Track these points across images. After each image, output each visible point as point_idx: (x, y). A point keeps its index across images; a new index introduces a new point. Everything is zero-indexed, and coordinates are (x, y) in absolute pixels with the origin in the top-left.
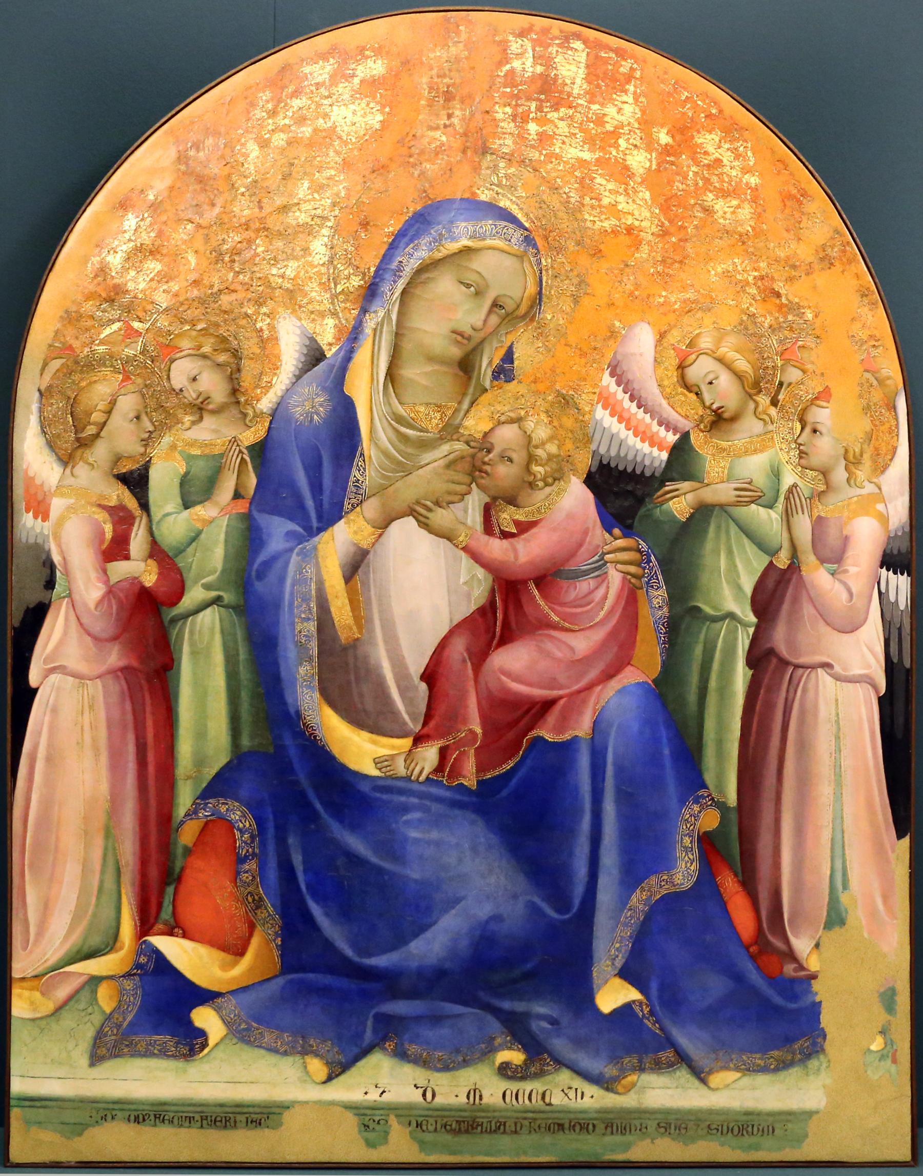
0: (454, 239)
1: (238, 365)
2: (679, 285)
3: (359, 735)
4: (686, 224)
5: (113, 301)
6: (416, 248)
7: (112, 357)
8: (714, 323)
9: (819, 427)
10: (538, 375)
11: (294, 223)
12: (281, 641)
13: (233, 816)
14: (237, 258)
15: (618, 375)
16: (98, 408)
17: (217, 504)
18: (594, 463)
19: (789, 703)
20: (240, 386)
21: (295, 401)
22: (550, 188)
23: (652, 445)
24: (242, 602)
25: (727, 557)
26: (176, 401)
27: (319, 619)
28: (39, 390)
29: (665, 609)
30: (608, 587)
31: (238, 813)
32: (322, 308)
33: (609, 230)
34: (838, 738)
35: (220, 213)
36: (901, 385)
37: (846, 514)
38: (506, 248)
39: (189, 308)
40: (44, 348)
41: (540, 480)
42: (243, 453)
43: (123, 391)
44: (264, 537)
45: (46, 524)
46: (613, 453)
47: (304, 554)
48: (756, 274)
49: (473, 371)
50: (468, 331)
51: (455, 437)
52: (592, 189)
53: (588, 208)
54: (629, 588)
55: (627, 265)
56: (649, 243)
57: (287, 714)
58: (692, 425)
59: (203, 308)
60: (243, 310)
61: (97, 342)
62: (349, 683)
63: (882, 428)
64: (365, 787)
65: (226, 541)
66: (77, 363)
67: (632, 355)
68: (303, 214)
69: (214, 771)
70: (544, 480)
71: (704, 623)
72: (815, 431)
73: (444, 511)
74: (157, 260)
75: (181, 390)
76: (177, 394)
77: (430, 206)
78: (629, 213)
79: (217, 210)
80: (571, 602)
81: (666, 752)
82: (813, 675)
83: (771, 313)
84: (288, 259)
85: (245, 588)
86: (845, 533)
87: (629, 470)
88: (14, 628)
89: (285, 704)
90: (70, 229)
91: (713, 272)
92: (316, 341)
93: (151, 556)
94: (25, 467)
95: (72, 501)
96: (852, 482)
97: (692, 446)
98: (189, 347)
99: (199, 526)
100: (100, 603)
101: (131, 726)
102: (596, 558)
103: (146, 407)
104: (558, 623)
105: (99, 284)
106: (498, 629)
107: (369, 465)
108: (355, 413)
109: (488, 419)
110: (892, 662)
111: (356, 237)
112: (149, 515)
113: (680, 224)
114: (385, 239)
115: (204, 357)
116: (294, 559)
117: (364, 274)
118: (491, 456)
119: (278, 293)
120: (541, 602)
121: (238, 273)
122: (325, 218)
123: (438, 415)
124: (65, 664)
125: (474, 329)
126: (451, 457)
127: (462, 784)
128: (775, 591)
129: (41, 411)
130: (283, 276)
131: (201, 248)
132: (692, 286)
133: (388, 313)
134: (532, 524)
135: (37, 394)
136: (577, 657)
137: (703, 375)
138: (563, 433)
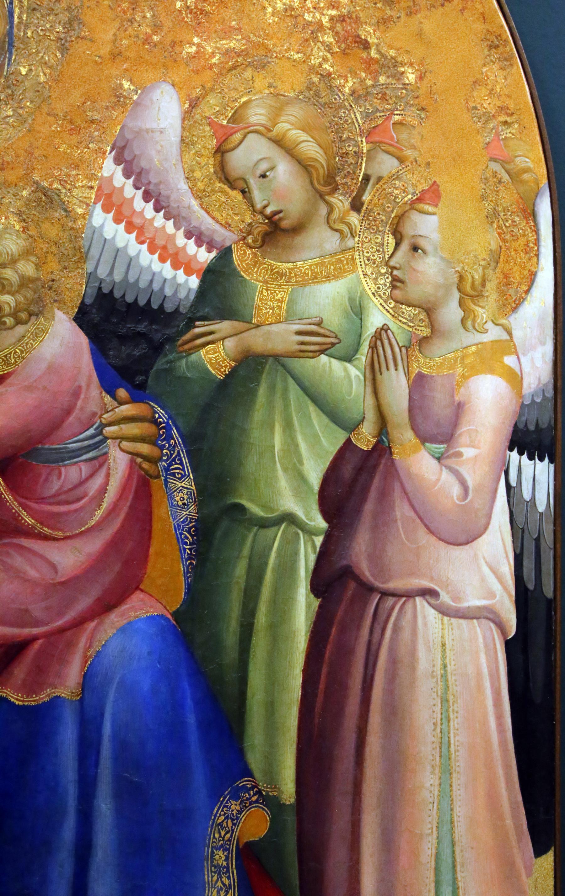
8: (270, 86)
9: (422, 243)
15: (126, 162)
18: (89, 291)
19: (374, 648)
23: (176, 266)
25: (284, 431)
29: (192, 508)
30: (108, 475)
34: (445, 700)
36: (545, 181)
37: (459, 370)
41: (9, 315)
48: (334, 12)
54: (140, 476)
58: (235, 238)
63: (515, 245)
70: (14, 314)
71: (249, 530)
72: (415, 248)
80: (54, 496)
81: (191, 719)
82: (409, 606)
83: (355, 74)
86: (457, 398)
87: (142, 302)
91: (270, 10)
96: (469, 323)
97: (235, 269)
102: (91, 431)
104: (33, 527)
110: (526, 589)
128: (355, 480)
132: (240, 29)
136: (60, 579)
137: (251, 164)
138: (45, 247)
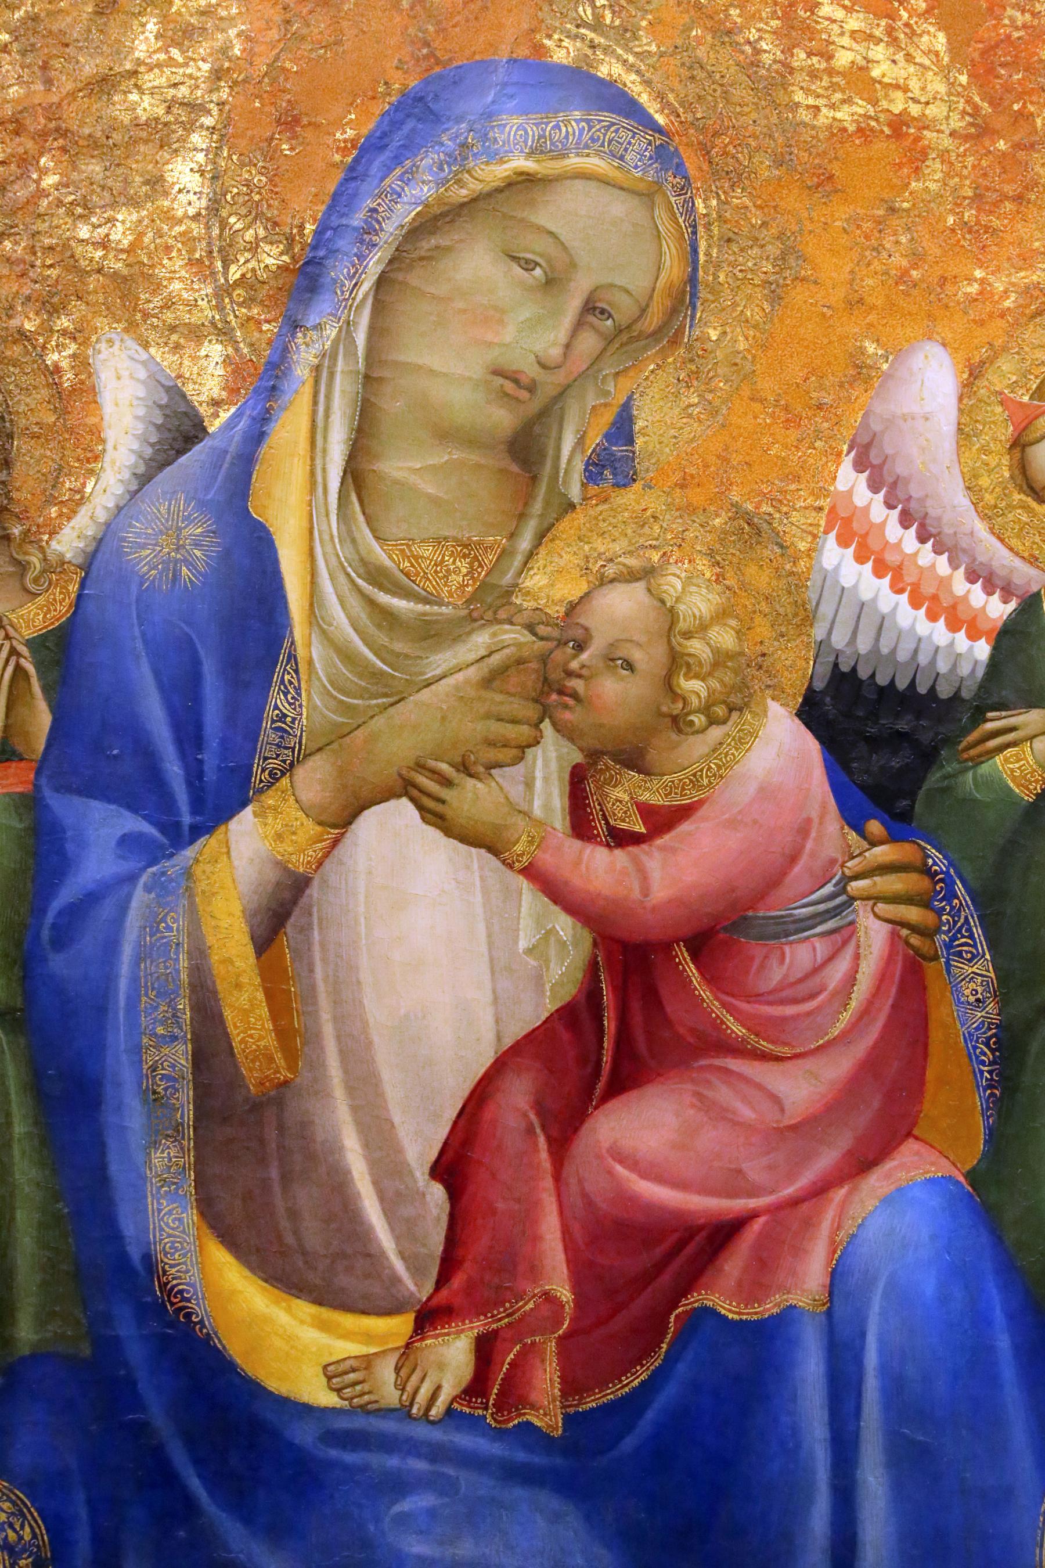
0: (496, 157)
2: (1014, 251)
3: (289, 1310)
4: (1032, 108)
6: (408, 178)
10: (692, 470)
12: (109, 1090)
15: (873, 466)
21: (138, 535)
22: (714, 31)
23: (953, 626)
24: (19, 1002)
27: (196, 1040)
29: (991, 1007)
30: (857, 957)
32: (195, 319)
33: (852, 128)
38: (616, 175)
41: (698, 711)
42: (19, 655)
44: (70, 847)
46: (863, 645)
47: (160, 887)
49: (541, 462)
50: (530, 370)
51: (502, 614)
52: (809, 31)
53: (801, 78)
54: (906, 956)
55: (892, 210)
56: (943, 156)
57: (122, 1262)
60: (14, 323)
62: (265, 1185)
64: (304, 1435)
67: (904, 418)
70: (706, 710)
73: (479, 785)
77: (440, 77)
78: (897, 87)
80: (770, 993)
81: (1003, 1343)
84: (114, 205)
87: (902, 684)
89: (115, 1236)
92: (184, 396)
102: (829, 888)
106: (607, 1058)
107: (309, 680)
108: (276, 562)
109: (576, 573)
111: (271, 154)
113: (1016, 107)
114: (337, 158)
116: (140, 898)
117: (290, 240)
118: (584, 656)
119: (93, 282)
120: (705, 993)
122: (196, 108)
123: (463, 566)
125: (543, 366)
126: (496, 659)
127: (529, 1424)
134: (684, 812)
136: (787, 1122)
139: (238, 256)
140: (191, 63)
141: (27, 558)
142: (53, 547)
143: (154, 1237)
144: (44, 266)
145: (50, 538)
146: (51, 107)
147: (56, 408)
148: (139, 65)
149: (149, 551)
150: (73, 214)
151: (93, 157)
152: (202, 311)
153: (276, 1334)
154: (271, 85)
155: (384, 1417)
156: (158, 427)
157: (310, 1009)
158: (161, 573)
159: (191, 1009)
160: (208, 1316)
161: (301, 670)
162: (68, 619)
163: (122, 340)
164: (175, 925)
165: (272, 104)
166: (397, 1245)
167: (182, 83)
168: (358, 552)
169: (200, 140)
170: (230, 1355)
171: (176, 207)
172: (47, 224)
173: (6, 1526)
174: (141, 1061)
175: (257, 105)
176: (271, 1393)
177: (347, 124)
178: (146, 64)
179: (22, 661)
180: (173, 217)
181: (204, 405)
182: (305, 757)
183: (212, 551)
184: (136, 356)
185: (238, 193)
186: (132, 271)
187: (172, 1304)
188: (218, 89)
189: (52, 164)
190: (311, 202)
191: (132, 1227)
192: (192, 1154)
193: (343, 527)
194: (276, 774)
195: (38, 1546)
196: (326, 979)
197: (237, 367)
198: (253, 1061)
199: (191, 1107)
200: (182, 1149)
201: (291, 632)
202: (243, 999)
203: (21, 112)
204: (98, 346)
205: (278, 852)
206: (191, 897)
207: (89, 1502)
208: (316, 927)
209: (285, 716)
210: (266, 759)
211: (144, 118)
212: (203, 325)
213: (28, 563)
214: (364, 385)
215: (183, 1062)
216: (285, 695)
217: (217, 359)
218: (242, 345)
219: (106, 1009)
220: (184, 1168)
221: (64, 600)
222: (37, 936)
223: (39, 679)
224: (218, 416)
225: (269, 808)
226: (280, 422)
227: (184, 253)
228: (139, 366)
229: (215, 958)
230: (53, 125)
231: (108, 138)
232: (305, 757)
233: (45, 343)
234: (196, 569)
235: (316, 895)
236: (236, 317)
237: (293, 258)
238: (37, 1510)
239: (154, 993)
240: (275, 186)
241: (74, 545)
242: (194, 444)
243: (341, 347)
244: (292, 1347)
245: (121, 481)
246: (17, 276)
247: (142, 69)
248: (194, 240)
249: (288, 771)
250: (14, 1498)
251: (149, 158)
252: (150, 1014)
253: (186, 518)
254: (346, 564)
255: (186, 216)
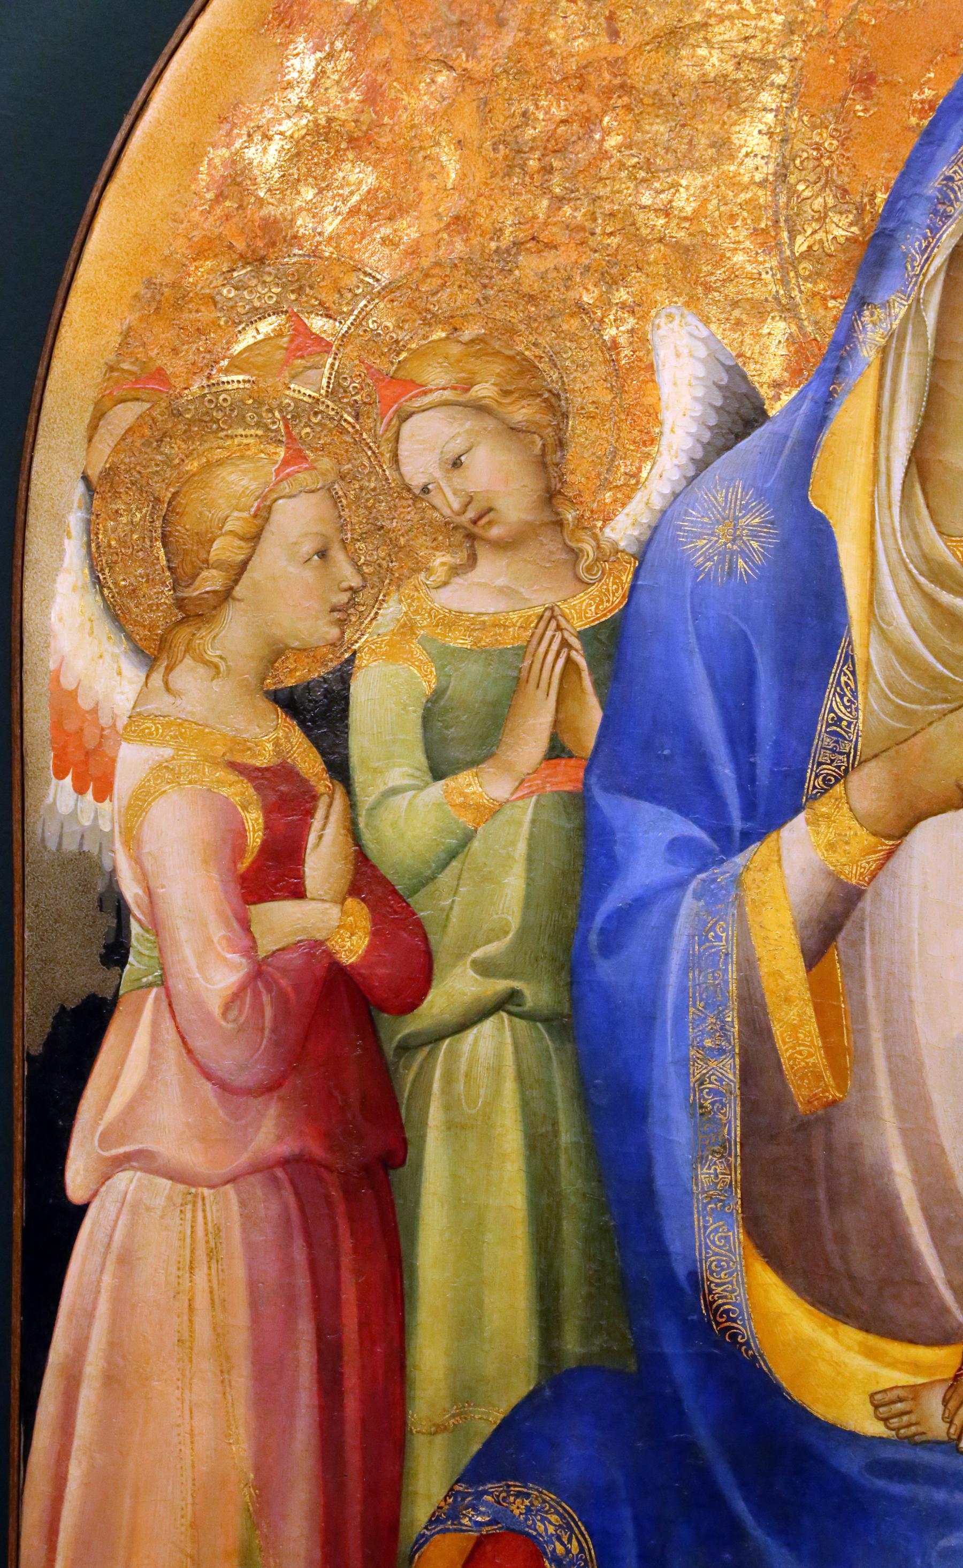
1: (558, 429)
3: (835, 1335)
5: (262, 260)
7: (259, 402)
11: (693, 74)
12: (655, 1101)
13: (540, 1527)
14: (556, 164)
16: (228, 527)
17: (508, 768)
20: (564, 483)
24: (566, 1009)
26: (413, 516)
28: (85, 478)
31: (554, 1518)
32: (759, 293)
35: (517, 45)
39: (444, 285)
40: (96, 374)
42: (570, 647)
43: (286, 488)
44: (619, 850)
45: (106, 805)
57: (668, 1281)
59: (477, 286)
60: (572, 295)
61: (225, 363)
65: (530, 860)
66: (177, 414)
68: (716, 53)
69: (497, 1415)
74: (367, 161)
75: (425, 490)
76: (416, 498)
79: (508, 39)
84: (677, 168)
85: (572, 972)
88: (30, 1058)
89: (661, 1252)
90: (154, 72)
92: (744, 377)
93: (354, 890)
94: (52, 666)
95: (168, 752)
98: (442, 382)
99: (466, 820)
100: (236, 997)
101: (305, 1300)
103: (342, 529)
105: (228, 217)
107: (866, 682)
108: (836, 556)
112: (349, 791)
114: (913, 120)
115: (480, 408)
116: (689, 905)
117: (861, 209)
119: (654, 252)
121: (561, 199)
124: (150, 1146)
129: (90, 529)
130: (666, 212)
131: (474, 134)
133: (917, 309)
135: (80, 488)
139: (806, 227)
140: (764, 15)
141: (580, 545)
142: (606, 535)
143: (700, 1254)
144: (604, 233)
145: (604, 526)
146: (616, 61)
147: (612, 386)
148: (710, 17)
149: (705, 542)
150: (636, 178)
151: (657, 116)
152: (766, 285)
153: (824, 1360)
154: (846, 40)
155: (931, 1449)
156: (718, 410)
157: (860, 1027)
158: (716, 565)
159: (740, 1023)
160: (753, 1338)
161: (857, 672)
162: (621, 610)
163: (682, 315)
164: (724, 935)
165: (847, 60)
166: (946, 1274)
167: (754, 37)
168: (920, 547)
169: (770, 99)
170: (775, 1379)
171: (742, 171)
172: (609, 189)
173: (554, 1538)
174: (688, 1074)
175: (832, 61)
176: (817, 1419)
177: (925, 83)
178: (716, 16)
179: (574, 654)
180: (739, 183)
181: (765, 386)
182: (860, 763)
183: (769, 543)
184: (696, 333)
185: (807, 158)
186: (694, 242)
187: (718, 1324)
188: (790, 44)
189: (616, 124)
190: (884, 168)
191: (678, 1243)
192: (739, 1172)
193: (905, 521)
194: (830, 780)
195: (585, 1561)
196: (877, 996)
197: (801, 346)
198: (802, 1078)
199: (738, 1123)
200: (729, 1166)
201: (849, 631)
202: (792, 1014)
203: (585, 67)
204: (657, 322)
205: (831, 863)
206: (741, 906)
207: (636, 1518)
208: (867, 942)
209: (841, 719)
210: (820, 764)
211: (712, 75)
212: (766, 300)
213: (581, 550)
214: (933, 368)
215: (731, 1077)
216: (842, 698)
217: (779, 338)
218: (806, 323)
219: (654, 1018)
220: (731, 1185)
221: (617, 590)
222: (585, 941)
223: (590, 674)
224: (780, 399)
225: (822, 816)
226: (843, 406)
227: (749, 222)
228: (700, 344)
229: (764, 970)
230: (617, 81)
231: (674, 96)
232: (860, 763)
233: (603, 317)
234: (753, 562)
235: (868, 909)
236: (801, 292)
237: (862, 229)
238: (583, 1523)
239: (702, 1004)
240: (847, 150)
241: (629, 532)
242: (754, 428)
243: (910, 326)
244: (839, 1373)
245: (678, 466)
246: (577, 244)
247: (712, 21)
248: (760, 208)
249: (842, 777)
250: (561, 1511)
251: (716, 118)
252: (698, 1026)
253: (743, 507)
254: (908, 561)
255: (752, 182)
